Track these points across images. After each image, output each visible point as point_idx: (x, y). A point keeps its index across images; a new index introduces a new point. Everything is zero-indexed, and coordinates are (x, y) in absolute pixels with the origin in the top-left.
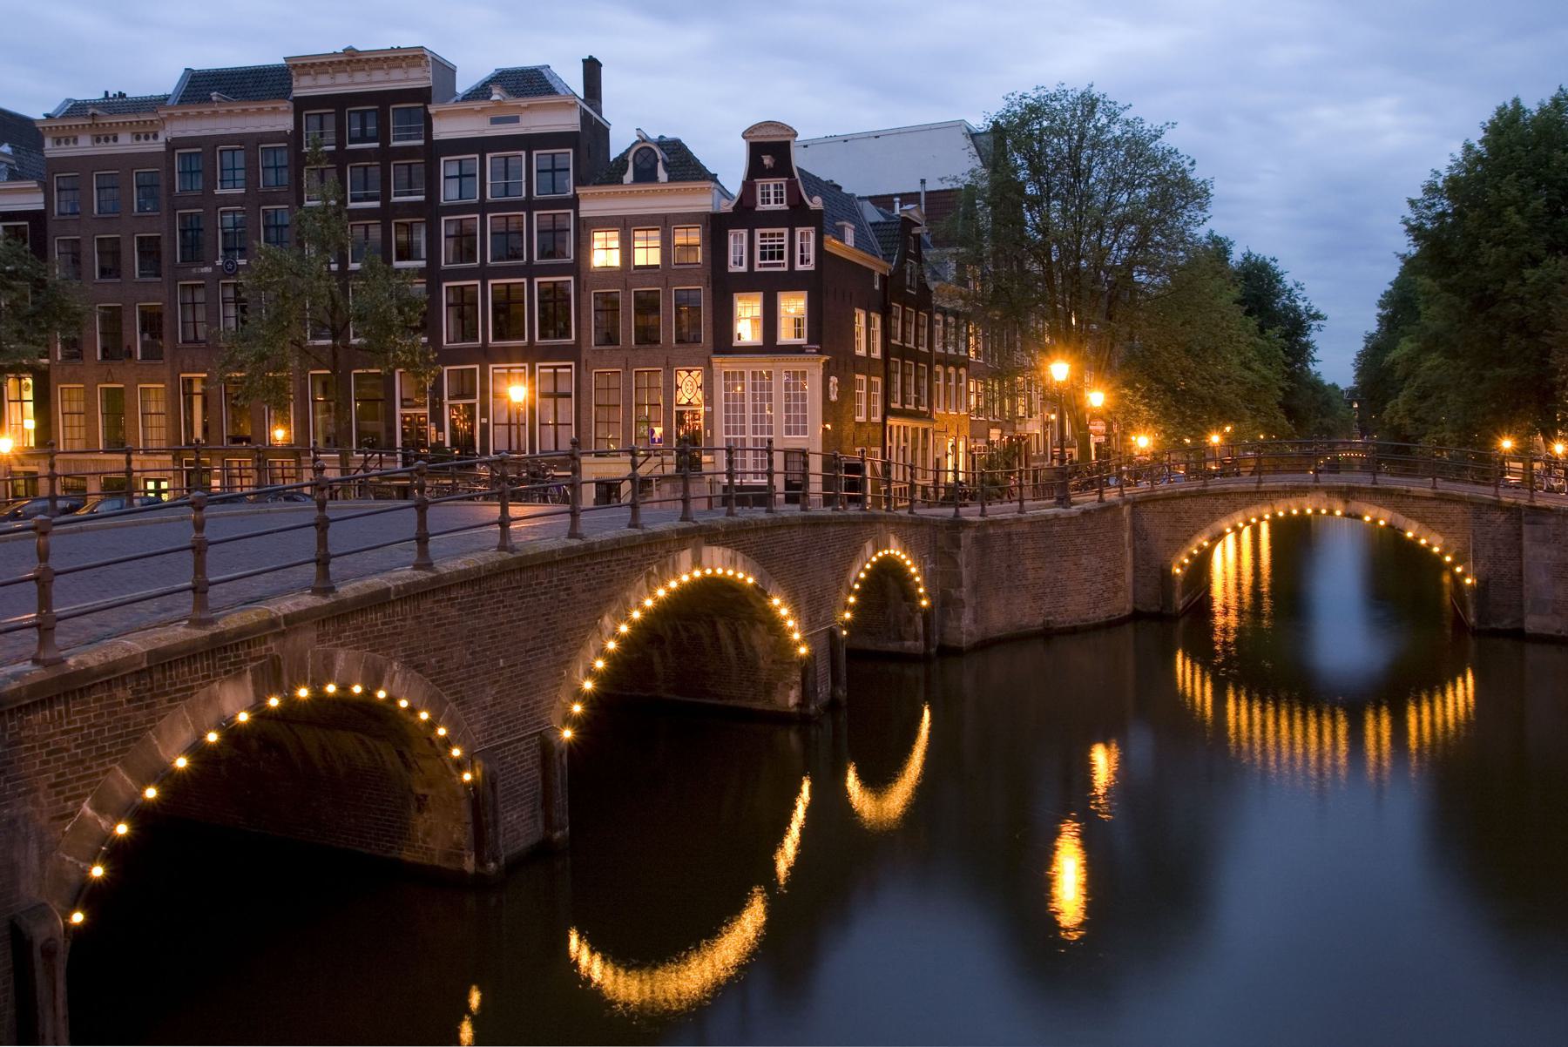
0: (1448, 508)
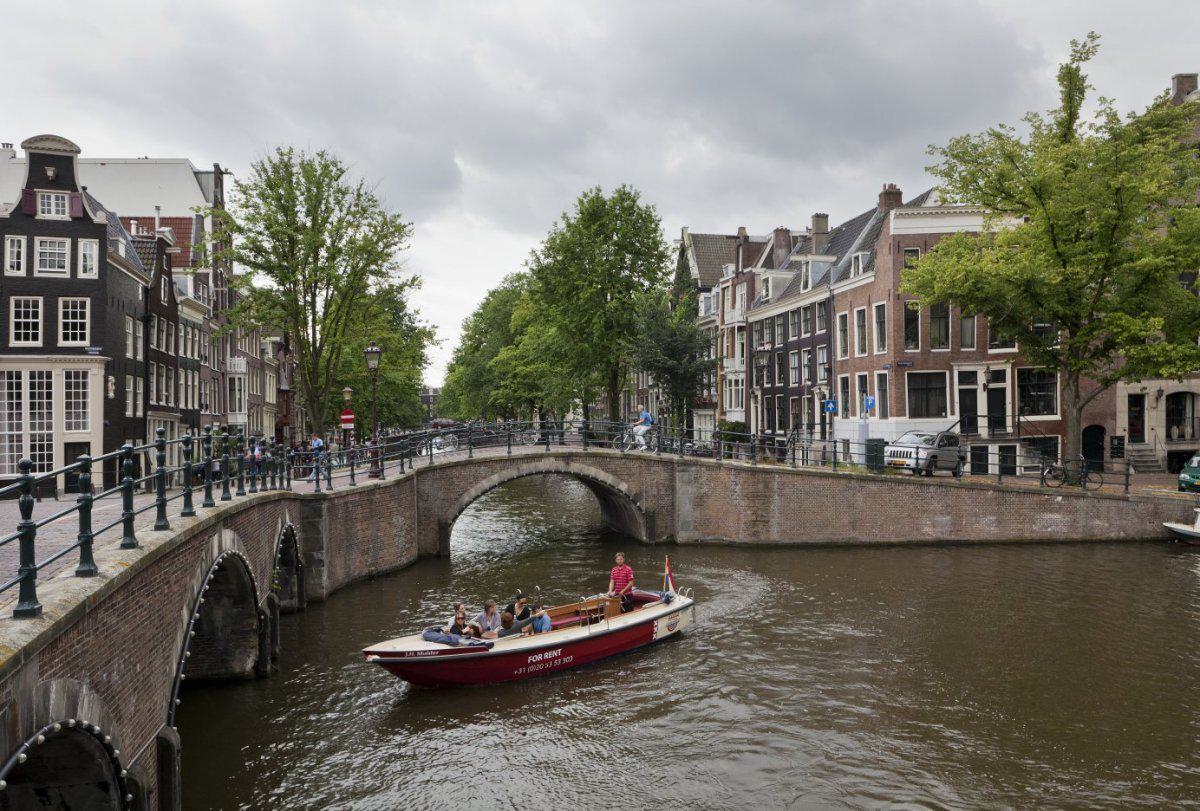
0: (630, 464)
